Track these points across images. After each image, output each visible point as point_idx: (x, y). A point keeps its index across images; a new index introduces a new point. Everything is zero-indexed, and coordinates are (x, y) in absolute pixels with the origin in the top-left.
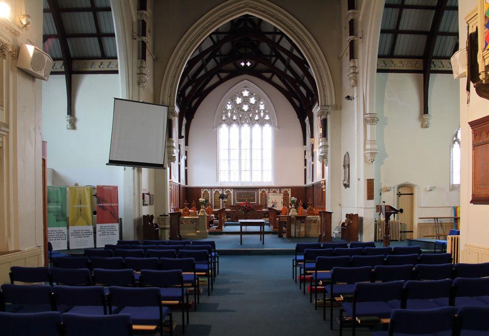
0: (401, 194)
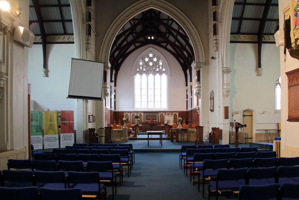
0: (245, 116)
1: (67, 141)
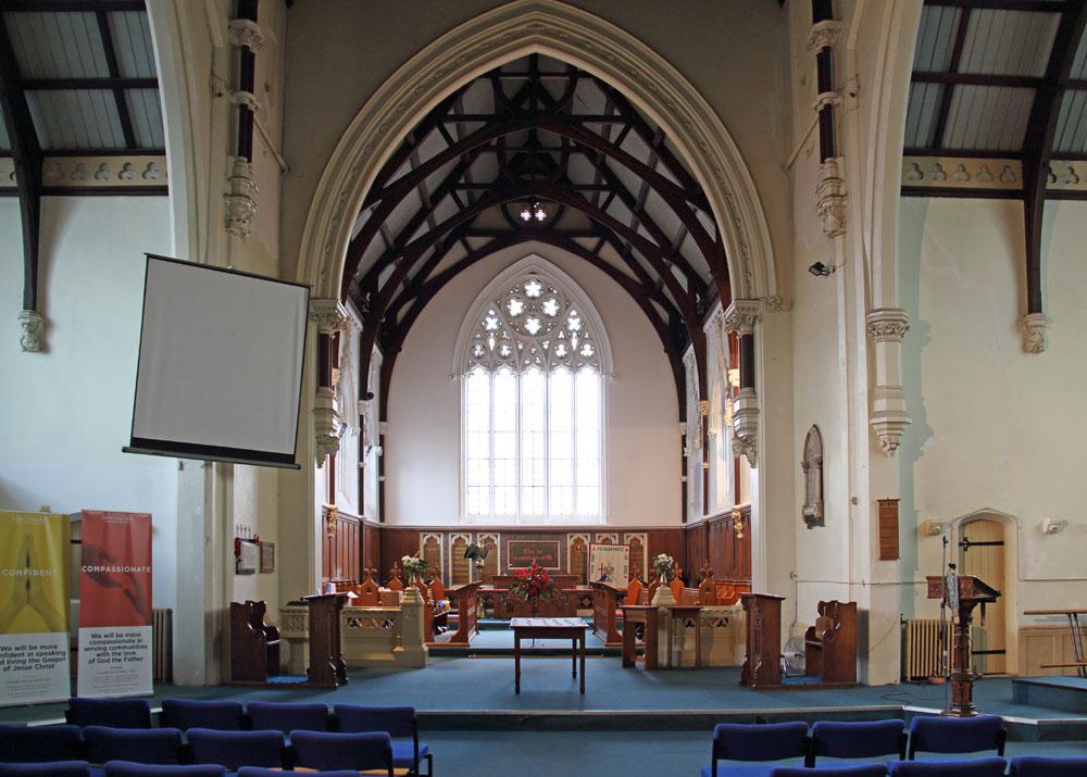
0: (970, 544)
1: (119, 670)
